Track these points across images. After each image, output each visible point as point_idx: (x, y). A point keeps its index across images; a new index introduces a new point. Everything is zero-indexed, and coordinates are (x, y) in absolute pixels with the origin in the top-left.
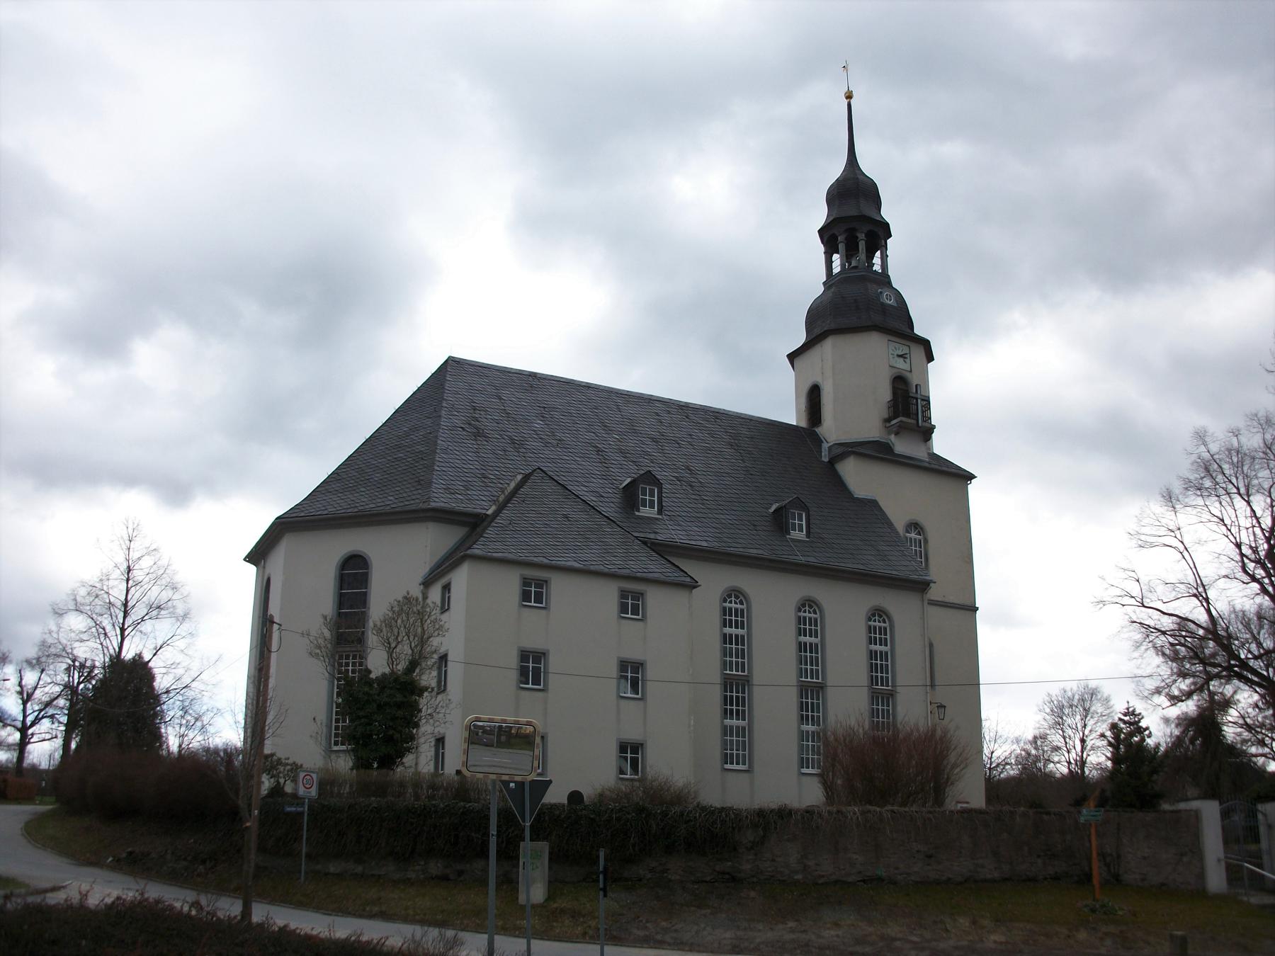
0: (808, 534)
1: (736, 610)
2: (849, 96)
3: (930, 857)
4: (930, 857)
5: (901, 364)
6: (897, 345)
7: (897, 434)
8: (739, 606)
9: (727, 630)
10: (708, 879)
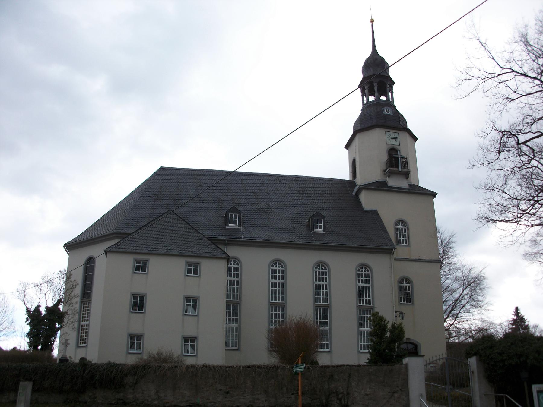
0: (324, 231)
1: (323, 272)
2: (372, 21)
3: (228, 393)
4: (228, 393)
5: (393, 142)
6: (391, 133)
7: (389, 176)
8: (280, 268)
9: (274, 281)
10: (113, 402)
